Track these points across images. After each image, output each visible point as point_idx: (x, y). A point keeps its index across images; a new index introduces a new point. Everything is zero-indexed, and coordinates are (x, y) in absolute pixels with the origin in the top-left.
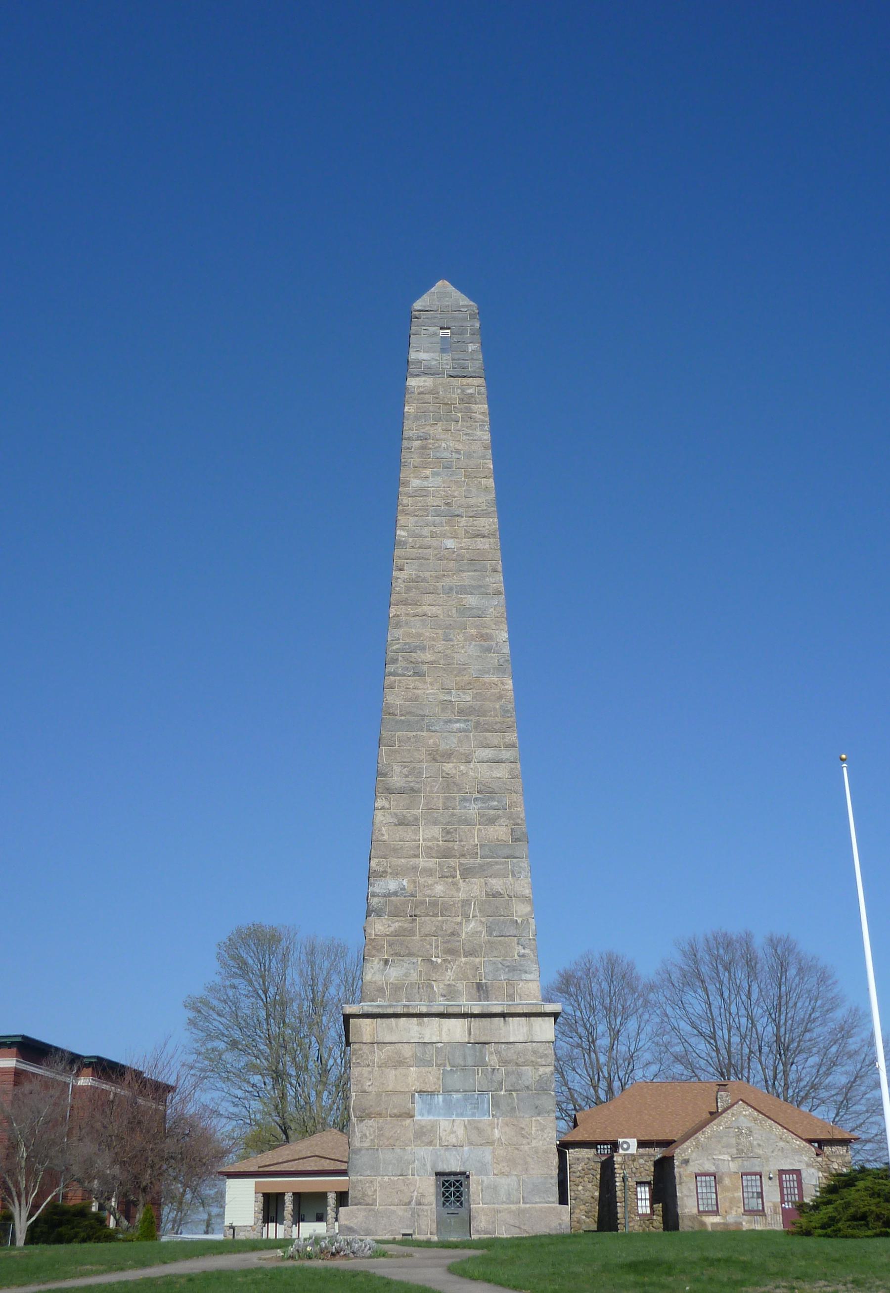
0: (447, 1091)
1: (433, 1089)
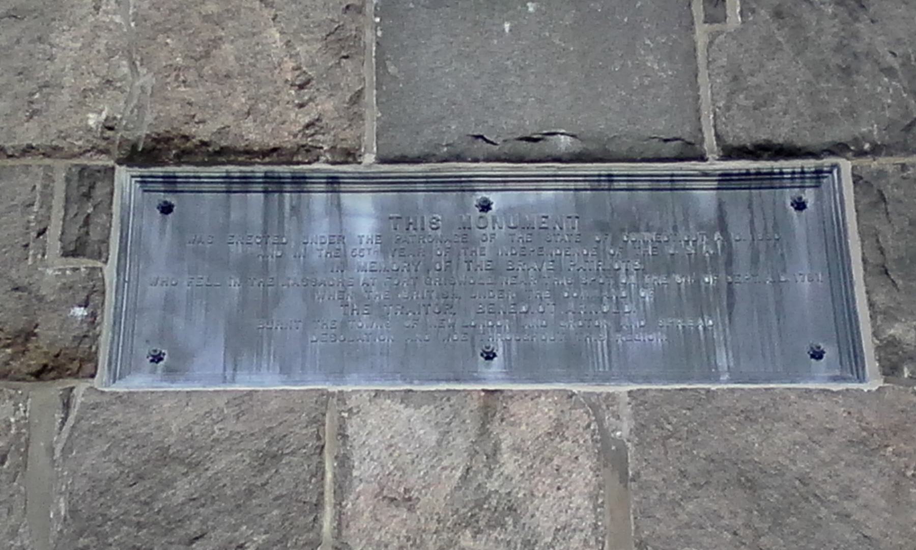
0: (419, 165)
1: (285, 125)
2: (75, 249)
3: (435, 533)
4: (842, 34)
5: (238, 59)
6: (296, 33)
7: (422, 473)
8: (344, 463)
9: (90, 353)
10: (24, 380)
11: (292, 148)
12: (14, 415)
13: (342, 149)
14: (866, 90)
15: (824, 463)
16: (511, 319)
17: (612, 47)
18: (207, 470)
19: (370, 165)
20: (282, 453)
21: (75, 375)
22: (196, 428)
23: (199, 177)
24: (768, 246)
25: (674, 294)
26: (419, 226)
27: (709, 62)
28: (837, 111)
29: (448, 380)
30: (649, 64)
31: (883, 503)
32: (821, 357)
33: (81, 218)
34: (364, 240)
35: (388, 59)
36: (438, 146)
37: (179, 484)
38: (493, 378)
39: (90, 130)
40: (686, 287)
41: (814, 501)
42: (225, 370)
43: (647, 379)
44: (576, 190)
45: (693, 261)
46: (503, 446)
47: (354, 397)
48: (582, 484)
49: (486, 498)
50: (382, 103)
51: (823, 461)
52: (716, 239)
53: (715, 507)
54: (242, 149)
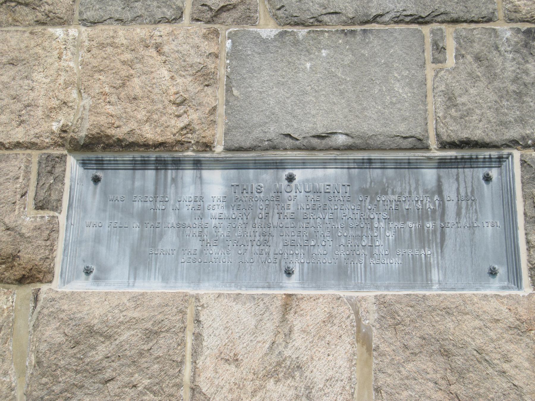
2: (40, 207)
3: (252, 381)
4: (518, 71)
5: (141, 88)
6: (177, 71)
7: (245, 344)
8: (198, 337)
9: (50, 269)
10: (12, 283)
11: (172, 143)
12: (6, 304)
13: (203, 142)
14: (530, 107)
15: (492, 340)
16: (304, 250)
17: (374, 78)
18: (116, 340)
19: (219, 153)
20: (161, 331)
21: (41, 281)
22: (110, 315)
23: (117, 161)
24: (467, 205)
25: (407, 235)
26: (249, 191)
27: (434, 88)
28: (512, 120)
29: (263, 287)
30: (396, 89)
31: (526, 364)
32: (496, 274)
33: (47, 185)
34: (215, 199)
35: (233, 86)
36: (262, 141)
37: (99, 348)
38: (292, 286)
39: (53, 133)
40: (415, 230)
41: (485, 363)
42: (129, 279)
43: (387, 288)
44: (348, 168)
45: (420, 213)
46: (296, 328)
47: (205, 297)
48: (344, 352)
49: (284, 360)
50: (229, 114)
51: (492, 339)
52: (435, 199)
53: (425, 367)
54: (142, 143)
